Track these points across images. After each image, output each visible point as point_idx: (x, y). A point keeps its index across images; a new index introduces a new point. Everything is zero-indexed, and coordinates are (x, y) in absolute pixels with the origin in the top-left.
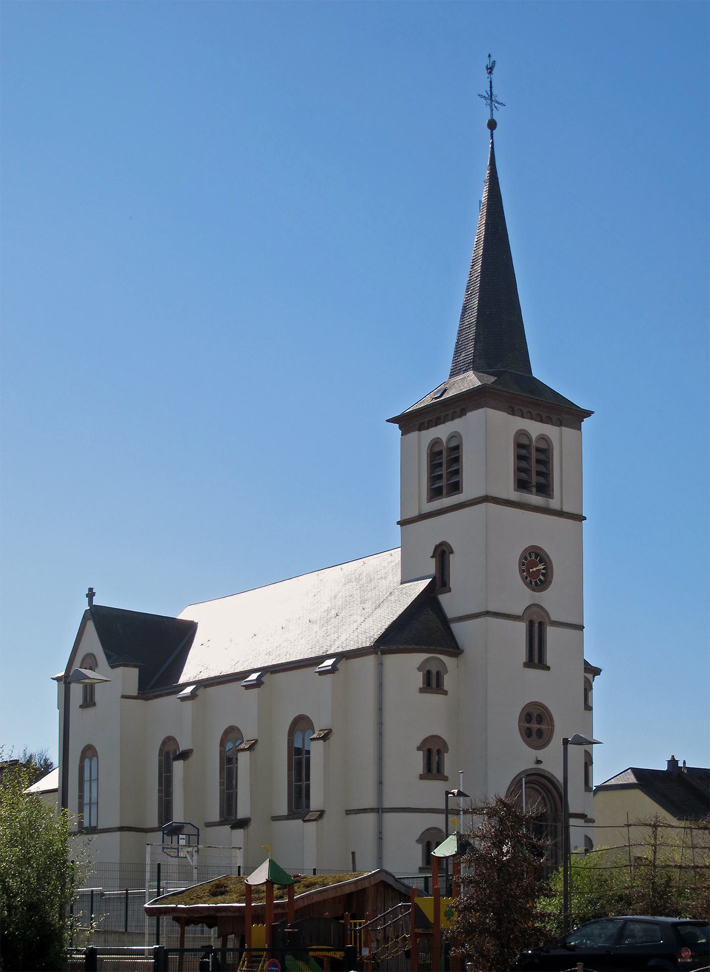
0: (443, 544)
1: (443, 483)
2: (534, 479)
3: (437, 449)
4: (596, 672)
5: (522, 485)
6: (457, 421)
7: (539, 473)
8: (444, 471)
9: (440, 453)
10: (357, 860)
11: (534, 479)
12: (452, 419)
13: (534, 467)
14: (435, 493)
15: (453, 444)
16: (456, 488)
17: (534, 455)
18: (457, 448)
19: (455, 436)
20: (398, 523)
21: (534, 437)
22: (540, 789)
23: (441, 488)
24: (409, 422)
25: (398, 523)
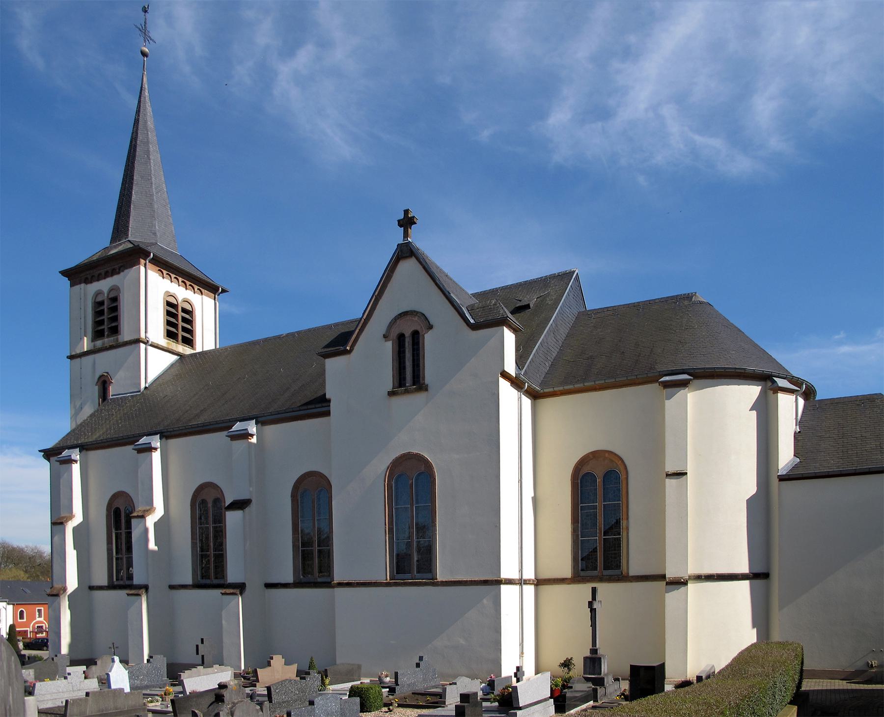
0: (118, 496)
1: (105, 327)
2: (181, 333)
3: (99, 299)
4: (85, 678)
5: (170, 335)
6: (115, 277)
7: (184, 329)
8: (105, 317)
9: (101, 303)
10: (362, 579)
11: (181, 333)
12: (112, 276)
13: (181, 324)
14: (98, 334)
15: (112, 295)
16: (115, 331)
17: (181, 314)
18: (115, 299)
19: (115, 289)
20: (68, 357)
21: (180, 299)
22: (231, 591)
23: (103, 320)
24: (78, 275)
25: (68, 357)
